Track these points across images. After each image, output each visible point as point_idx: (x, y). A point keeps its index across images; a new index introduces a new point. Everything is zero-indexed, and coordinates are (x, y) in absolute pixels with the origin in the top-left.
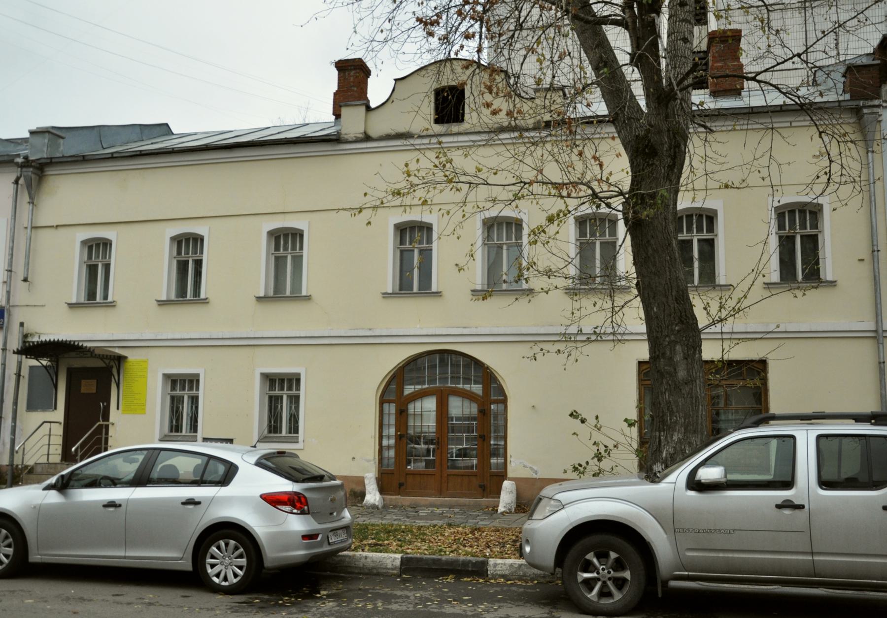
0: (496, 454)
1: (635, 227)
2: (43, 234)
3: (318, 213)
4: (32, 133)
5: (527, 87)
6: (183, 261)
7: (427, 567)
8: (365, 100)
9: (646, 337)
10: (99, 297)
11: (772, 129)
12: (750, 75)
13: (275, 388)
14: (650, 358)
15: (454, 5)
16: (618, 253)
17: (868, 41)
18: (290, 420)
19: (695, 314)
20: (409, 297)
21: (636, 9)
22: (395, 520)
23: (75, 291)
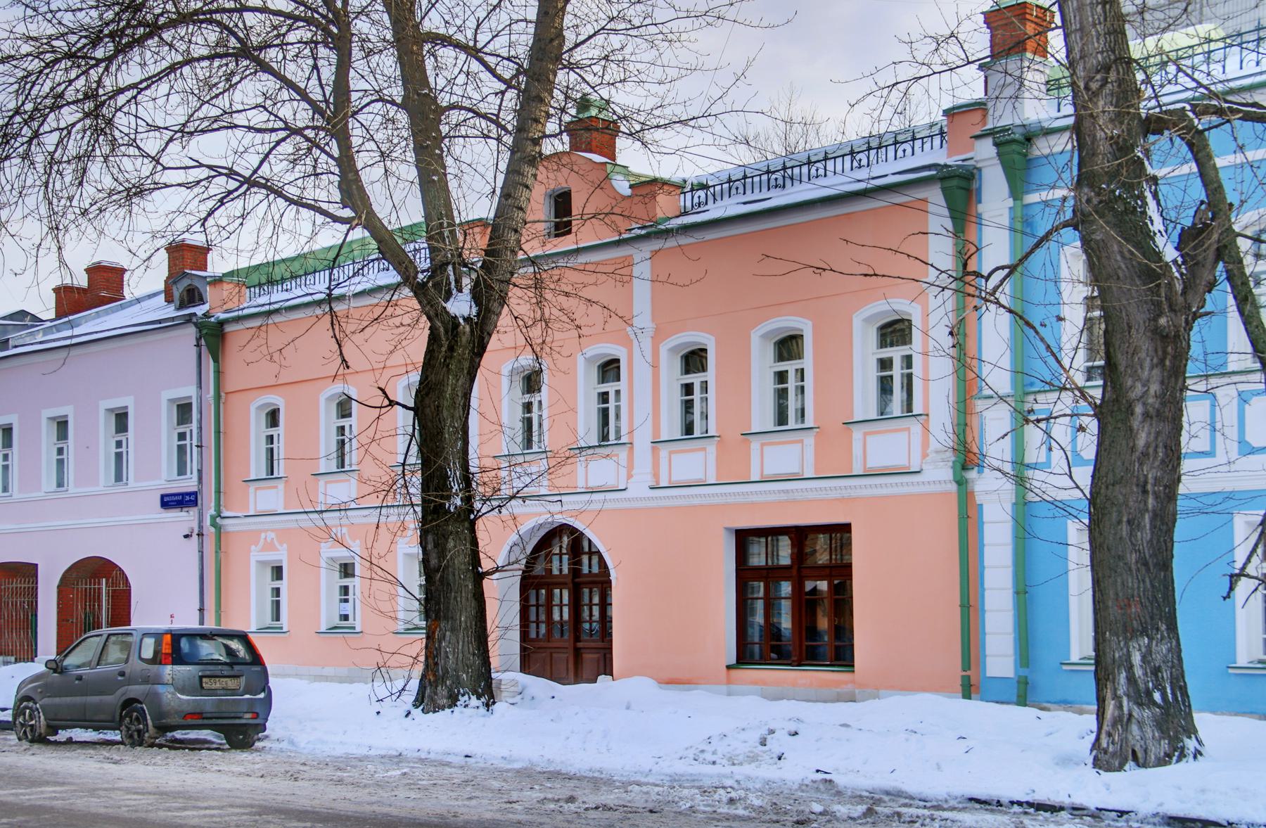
0: (436, 172)
1: (1095, 528)
2: (230, 395)
3: (304, 384)
4: (949, 113)
5: (97, 140)
6: (840, 660)
7: (417, 480)
8: (761, 658)
9: (1093, 662)
10: (612, 436)
11: (1240, 45)
12: (301, 24)
13: (437, 469)
14: (1235, 241)
15: (462, 112)
16: (198, 345)
17: (474, 166)
18: (99, 596)
19: (1174, 566)
20: (901, 468)
21: (247, 696)
22: (562, 635)
23: (671, 425)
